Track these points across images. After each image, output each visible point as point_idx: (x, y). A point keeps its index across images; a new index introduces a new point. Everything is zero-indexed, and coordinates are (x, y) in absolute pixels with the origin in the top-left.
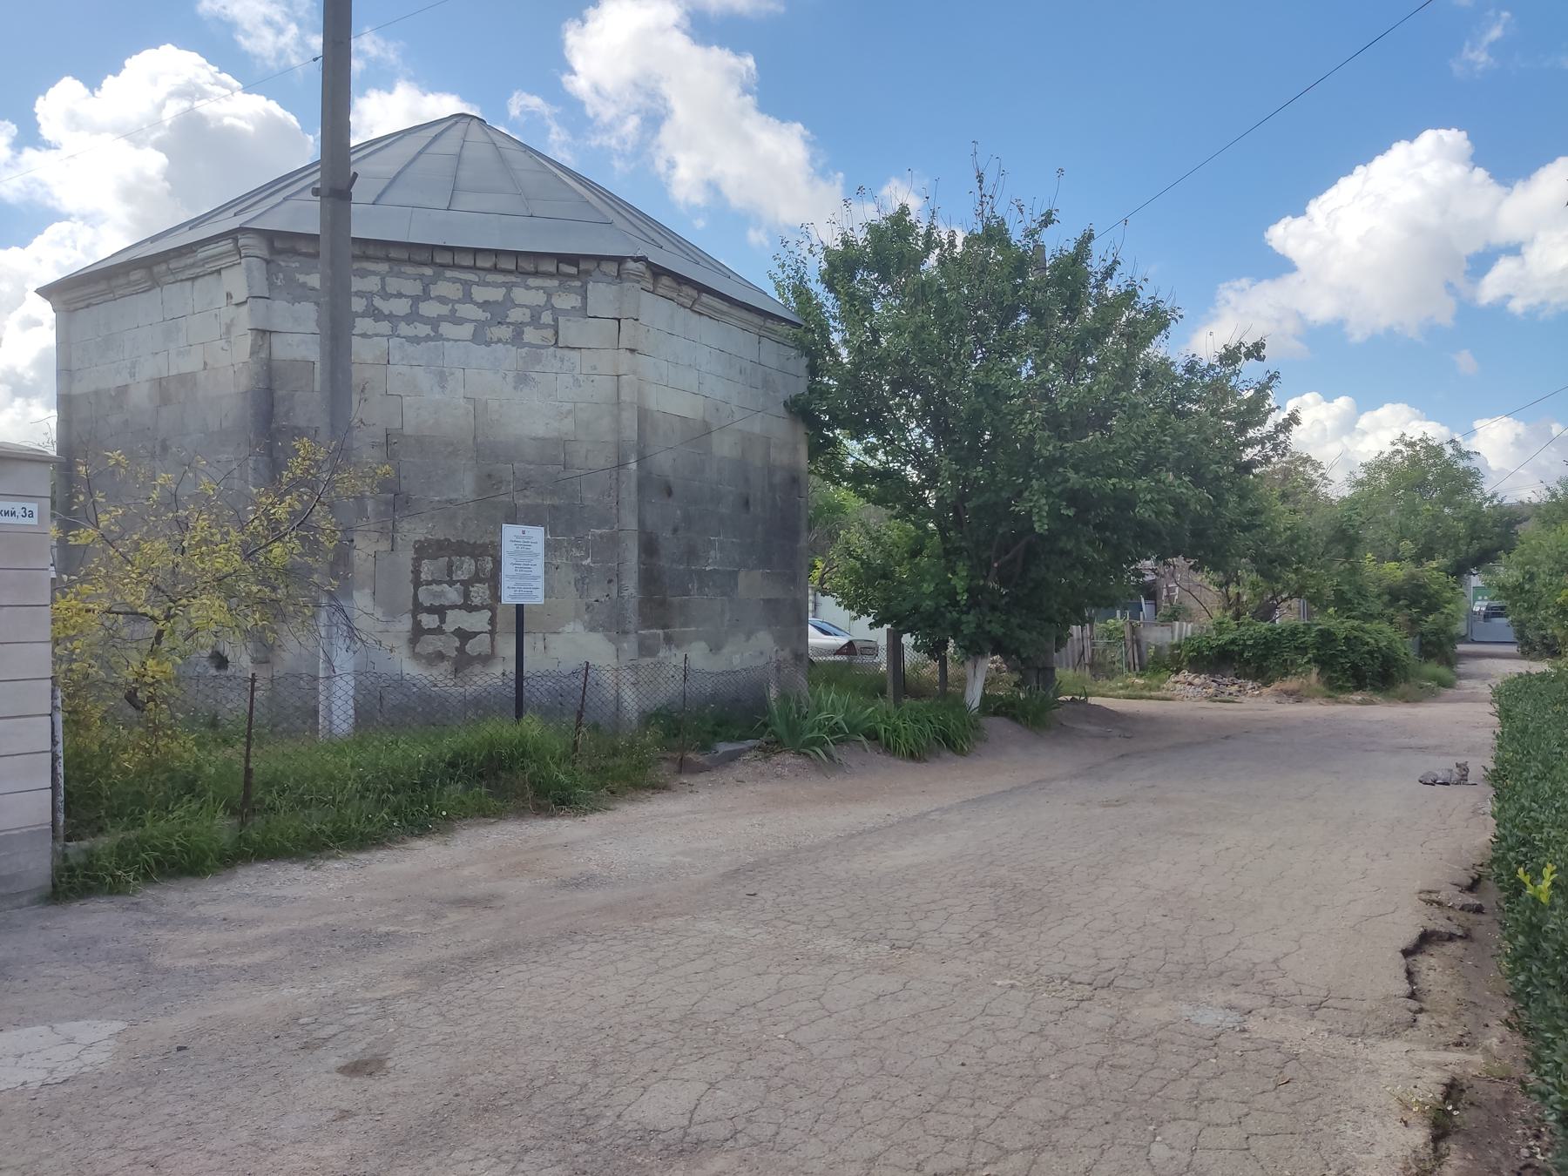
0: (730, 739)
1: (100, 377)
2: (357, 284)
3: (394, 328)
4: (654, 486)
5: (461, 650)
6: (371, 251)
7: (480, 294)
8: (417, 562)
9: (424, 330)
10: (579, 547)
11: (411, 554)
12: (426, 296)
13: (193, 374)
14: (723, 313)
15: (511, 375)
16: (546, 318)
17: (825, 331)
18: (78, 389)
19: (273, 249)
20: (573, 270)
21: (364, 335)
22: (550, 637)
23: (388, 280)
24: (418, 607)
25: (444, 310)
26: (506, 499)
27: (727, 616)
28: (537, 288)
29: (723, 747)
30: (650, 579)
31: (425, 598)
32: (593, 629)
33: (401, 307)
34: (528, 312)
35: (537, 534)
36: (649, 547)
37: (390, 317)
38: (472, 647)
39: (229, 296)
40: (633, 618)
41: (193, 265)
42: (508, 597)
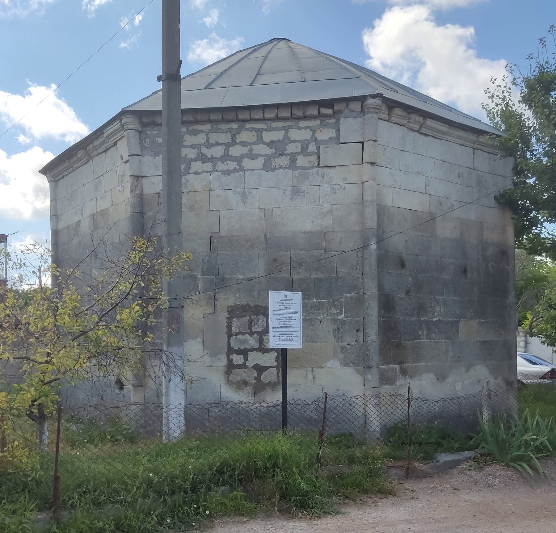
0: (450, 450)
1: (69, 218)
2: (189, 140)
3: (214, 166)
4: (390, 261)
5: (258, 379)
6: (199, 117)
7: (268, 137)
8: (230, 320)
9: (232, 165)
10: (336, 307)
11: (226, 315)
12: (234, 142)
13: (107, 209)
14: (445, 133)
15: (288, 190)
16: (312, 148)
17: (526, 142)
18: (61, 226)
19: (144, 125)
20: (329, 111)
21: (196, 173)
22: (316, 370)
23: (211, 135)
24: (230, 351)
25: (245, 150)
26: (284, 275)
27: (451, 354)
28: (306, 128)
29: (444, 458)
30: (388, 329)
31: (235, 345)
32: (346, 365)
33: (218, 152)
34: (299, 145)
35: (296, 297)
36: (387, 305)
37: (212, 160)
38: (266, 377)
39: (122, 158)
40: (375, 358)
41: (104, 142)
42: (275, 341)
